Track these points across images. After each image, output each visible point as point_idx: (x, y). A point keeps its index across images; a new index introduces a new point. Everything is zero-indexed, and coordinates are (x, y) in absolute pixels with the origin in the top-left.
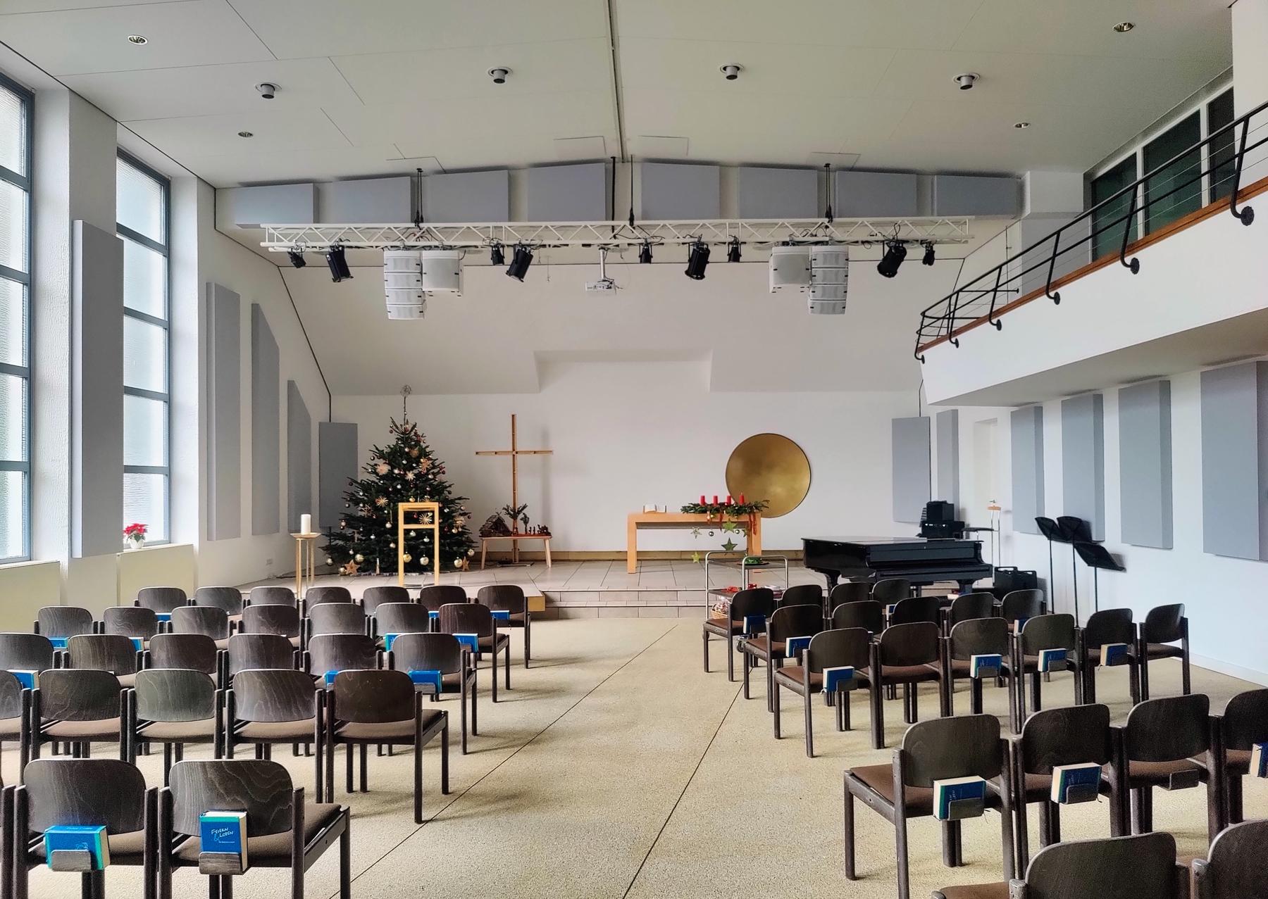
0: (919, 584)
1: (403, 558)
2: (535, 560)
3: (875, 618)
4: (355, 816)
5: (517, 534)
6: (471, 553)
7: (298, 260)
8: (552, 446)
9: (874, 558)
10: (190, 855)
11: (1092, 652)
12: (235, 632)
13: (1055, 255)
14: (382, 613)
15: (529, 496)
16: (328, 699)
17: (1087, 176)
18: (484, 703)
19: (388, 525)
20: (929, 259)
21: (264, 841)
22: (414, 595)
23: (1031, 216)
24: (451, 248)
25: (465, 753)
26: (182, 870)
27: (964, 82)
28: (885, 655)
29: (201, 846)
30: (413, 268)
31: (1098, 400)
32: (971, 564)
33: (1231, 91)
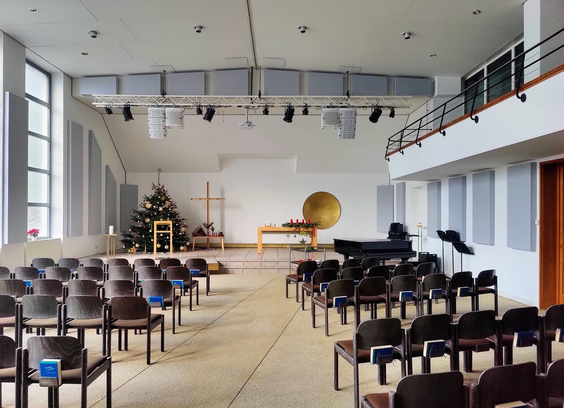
0: (384, 260)
1: (156, 246)
2: (217, 247)
3: (358, 275)
4: (113, 362)
5: (209, 236)
6: (188, 244)
7: (109, 111)
8: (226, 196)
9: (364, 248)
10: (35, 378)
11: (453, 291)
12: (74, 278)
13: (444, 114)
14: (140, 270)
15: (215, 218)
16: (109, 308)
17: (463, 79)
18: (185, 312)
19: (150, 231)
20: (392, 115)
21: (68, 373)
22: (157, 262)
23: (437, 97)
24: (179, 107)
25: (174, 333)
26: (33, 385)
27: (406, 36)
28: (361, 292)
29: (40, 375)
30: (161, 115)
31: (464, 179)
32: (407, 251)
33: (523, 42)
